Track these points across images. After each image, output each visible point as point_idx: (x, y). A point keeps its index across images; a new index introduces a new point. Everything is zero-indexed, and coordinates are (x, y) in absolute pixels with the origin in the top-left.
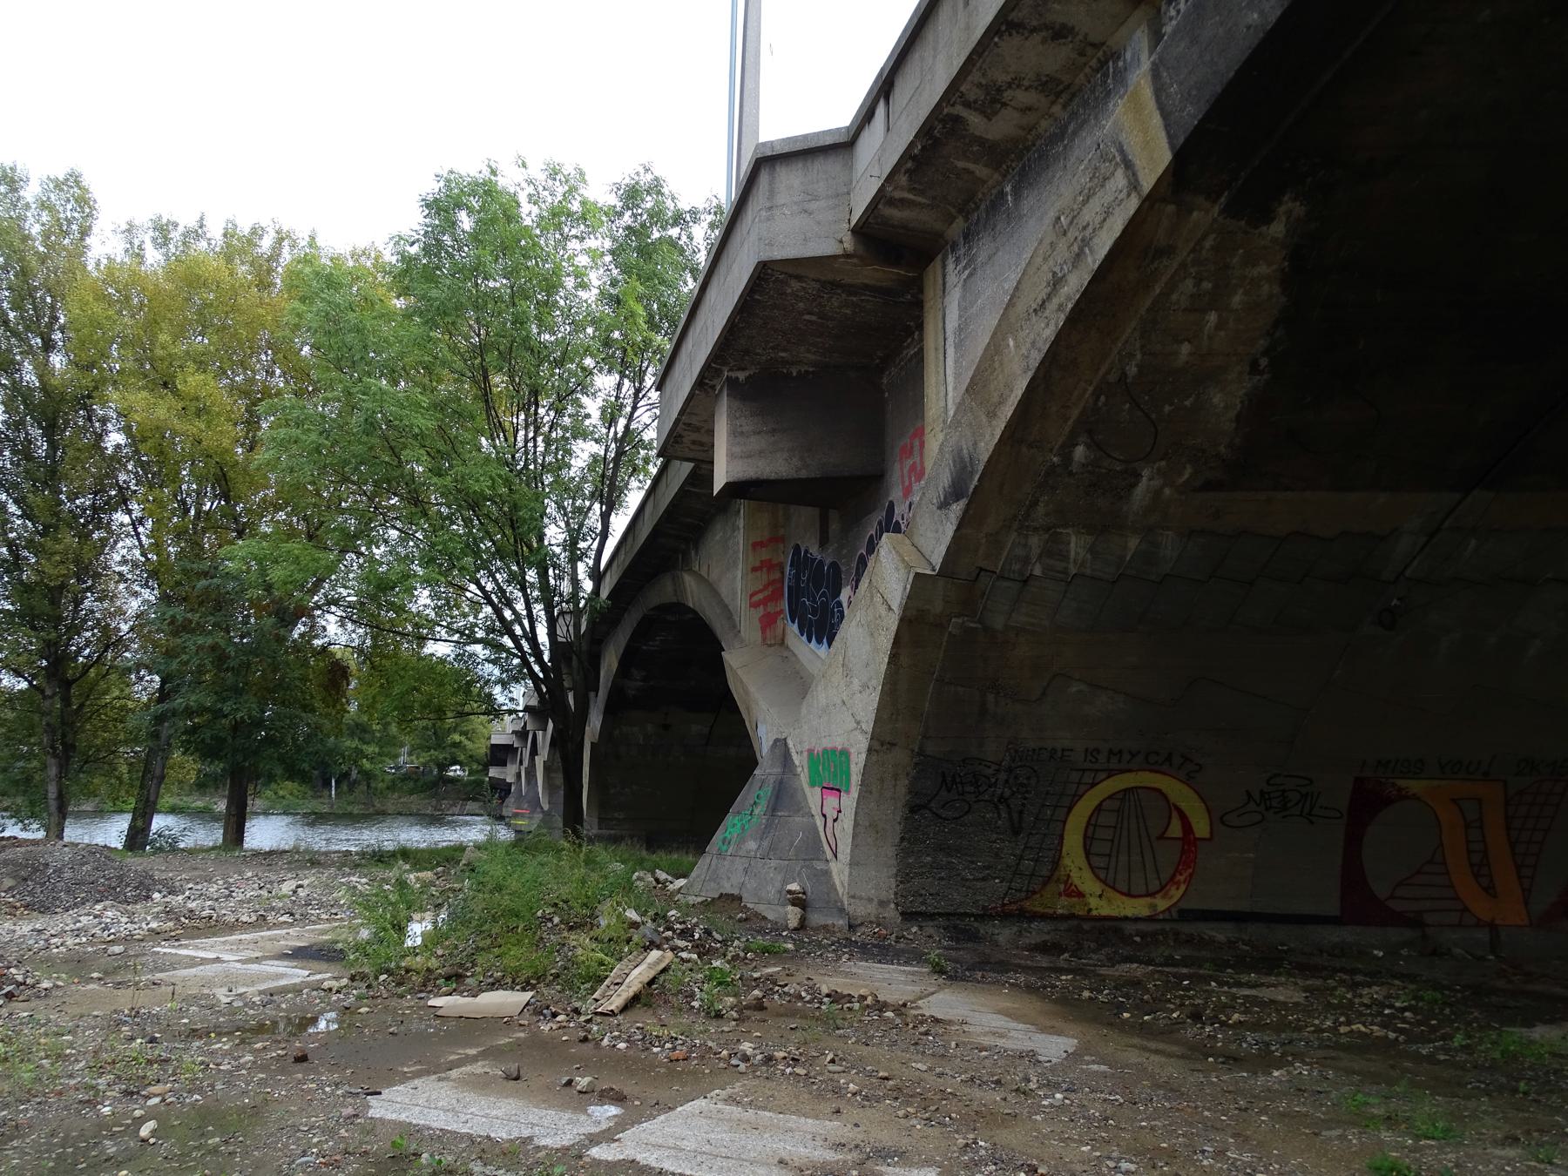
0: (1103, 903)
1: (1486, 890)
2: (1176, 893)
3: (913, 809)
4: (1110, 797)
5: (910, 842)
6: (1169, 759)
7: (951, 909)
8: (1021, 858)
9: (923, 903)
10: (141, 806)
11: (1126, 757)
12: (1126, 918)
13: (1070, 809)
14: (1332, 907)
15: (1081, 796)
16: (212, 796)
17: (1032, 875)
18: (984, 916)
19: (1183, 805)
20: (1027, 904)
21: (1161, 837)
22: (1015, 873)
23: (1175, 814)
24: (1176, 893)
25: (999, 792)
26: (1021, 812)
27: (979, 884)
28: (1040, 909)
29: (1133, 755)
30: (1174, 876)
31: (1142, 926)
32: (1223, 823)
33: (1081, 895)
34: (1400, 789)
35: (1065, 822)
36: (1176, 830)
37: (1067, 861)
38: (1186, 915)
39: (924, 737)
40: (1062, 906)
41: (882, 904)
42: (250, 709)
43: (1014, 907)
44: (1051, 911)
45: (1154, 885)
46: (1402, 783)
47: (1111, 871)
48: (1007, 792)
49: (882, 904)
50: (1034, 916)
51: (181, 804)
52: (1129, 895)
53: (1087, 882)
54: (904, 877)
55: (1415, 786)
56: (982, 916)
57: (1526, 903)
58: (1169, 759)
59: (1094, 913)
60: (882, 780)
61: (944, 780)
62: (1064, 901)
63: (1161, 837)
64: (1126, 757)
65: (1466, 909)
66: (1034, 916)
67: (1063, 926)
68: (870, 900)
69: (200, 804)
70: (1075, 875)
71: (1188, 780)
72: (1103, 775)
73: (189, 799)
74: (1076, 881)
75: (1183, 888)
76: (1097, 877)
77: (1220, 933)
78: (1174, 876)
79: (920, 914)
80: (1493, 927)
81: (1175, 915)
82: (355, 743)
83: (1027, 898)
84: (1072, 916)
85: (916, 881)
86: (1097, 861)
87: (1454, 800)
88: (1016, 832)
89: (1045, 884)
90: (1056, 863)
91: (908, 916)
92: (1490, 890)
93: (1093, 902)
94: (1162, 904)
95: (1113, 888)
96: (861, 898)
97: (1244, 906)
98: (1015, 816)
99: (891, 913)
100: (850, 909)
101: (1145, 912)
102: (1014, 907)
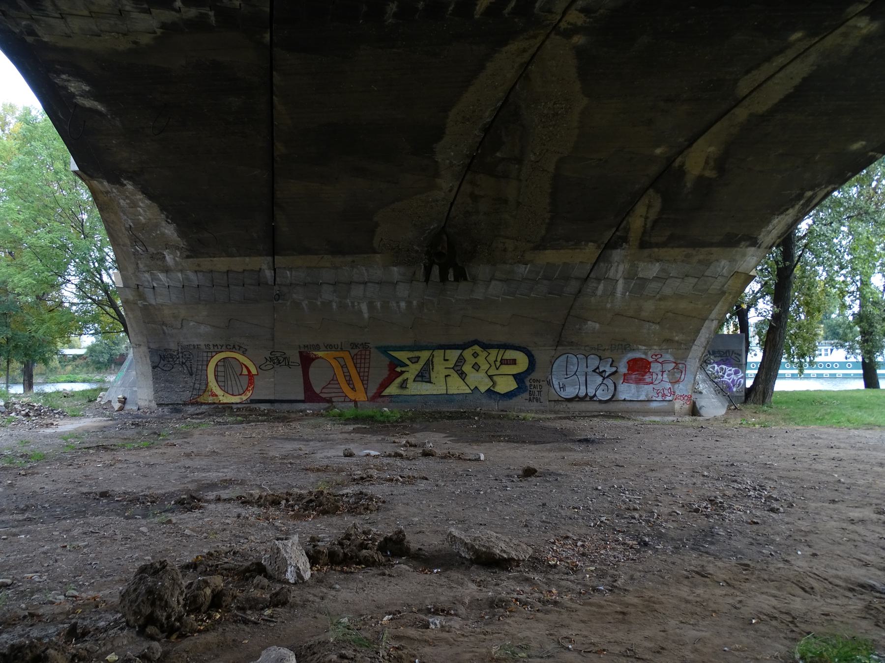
0: (224, 398)
1: (352, 389)
2: (249, 394)
3: (154, 368)
4: (219, 361)
5: (156, 379)
6: (234, 347)
7: (172, 402)
8: (195, 384)
9: (163, 400)
10: (26, 378)
11: (220, 347)
12: (233, 403)
13: (207, 365)
14: (302, 397)
15: (209, 361)
16: (104, 373)
17: (199, 389)
18: (185, 404)
19: (245, 363)
20: (198, 400)
21: (241, 374)
22: (194, 389)
23: (243, 366)
24: (249, 394)
25: (181, 360)
26: (191, 367)
27: (182, 393)
28: (203, 401)
29: (222, 346)
30: (247, 388)
31: (239, 406)
32: (261, 369)
33: (216, 396)
34: (315, 355)
35: (207, 370)
36: (245, 372)
37: (210, 384)
38: (253, 401)
39: (148, 342)
40: (211, 400)
41: (150, 401)
42: (7, 334)
43: (194, 401)
44: (207, 402)
45: (241, 392)
46: (314, 353)
47: (226, 387)
48: (184, 361)
49: (150, 401)
50: (202, 404)
51: (88, 378)
52: (233, 395)
53: (219, 392)
54: (156, 391)
55: (320, 354)
56: (185, 404)
57: (366, 393)
58: (234, 347)
59: (221, 402)
60: (141, 358)
61: (161, 357)
62: (211, 398)
63: (241, 374)
64: (220, 347)
65: (346, 396)
66: (202, 404)
67: (213, 406)
68: (146, 400)
69: (98, 377)
70: (214, 389)
71: (244, 354)
72: (214, 354)
73: (93, 375)
74: (215, 391)
75: (251, 392)
76: (221, 389)
77: (263, 407)
78: (247, 388)
79: (164, 404)
80: (355, 402)
81: (249, 402)
82: (866, 338)
83: (198, 397)
84: (214, 403)
85: (160, 393)
86: (220, 384)
87: (335, 358)
88: (191, 374)
89: (204, 392)
90: (207, 384)
91: (159, 405)
92: (353, 389)
93: (221, 398)
94: (244, 398)
95: (227, 393)
96: (143, 399)
97: (272, 398)
98: (189, 368)
99: (154, 405)
100: (139, 403)
101: (239, 401)
102: (194, 401)
